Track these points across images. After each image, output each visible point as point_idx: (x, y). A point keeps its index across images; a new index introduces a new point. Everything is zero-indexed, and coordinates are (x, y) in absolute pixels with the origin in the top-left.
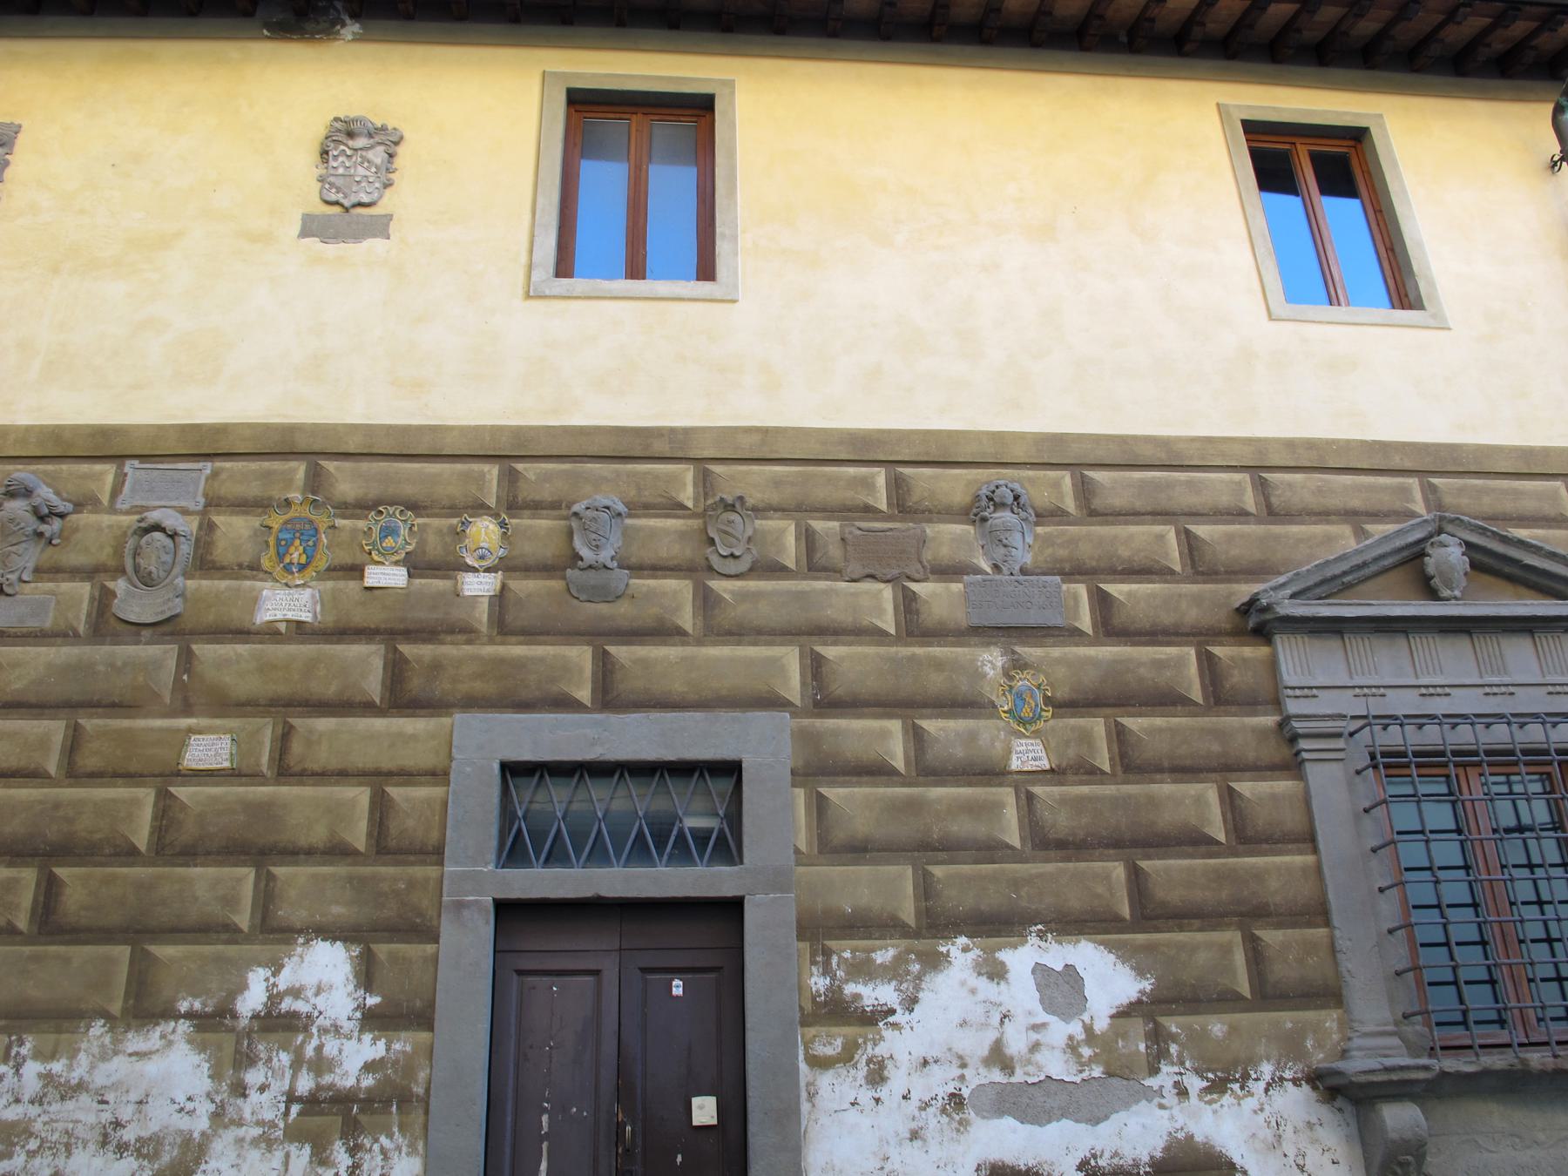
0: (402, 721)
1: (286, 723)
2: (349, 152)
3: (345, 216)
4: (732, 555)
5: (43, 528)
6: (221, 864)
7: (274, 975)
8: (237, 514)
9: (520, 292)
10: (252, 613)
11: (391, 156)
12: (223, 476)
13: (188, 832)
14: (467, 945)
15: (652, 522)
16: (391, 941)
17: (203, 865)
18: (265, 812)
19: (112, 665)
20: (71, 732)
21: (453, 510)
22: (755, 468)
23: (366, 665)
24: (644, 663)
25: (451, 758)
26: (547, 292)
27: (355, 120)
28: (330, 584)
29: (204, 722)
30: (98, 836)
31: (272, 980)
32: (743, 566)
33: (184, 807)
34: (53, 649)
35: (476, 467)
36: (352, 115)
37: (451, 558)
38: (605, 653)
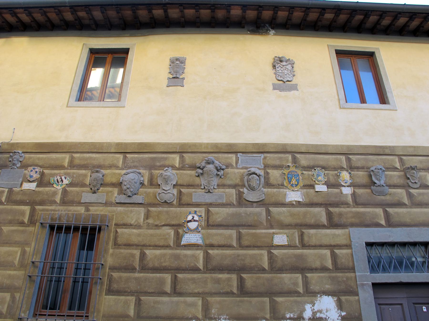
0: (334, 230)
1: (301, 231)
2: (282, 66)
3: (284, 84)
4: (415, 183)
5: (219, 173)
6: (291, 273)
7: (313, 306)
8: (274, 169)
9: (338, 107)
10: (285, 198)
11: (293, 67)
12: (268, 158)
13: (279, 264)
14: (366, 296)
15: (390, 173)
16: (345, 296)
17: (285, 274)
18: (300, 257)
19: (246, 214)
20: (238, 234)
21: (335, 169)
22: (414, 157)
23: (320, 214)
24: (397, 213)
25: (351, 241)
26: (346, 107)
27: (282, 57)
28: (305, 190)
29: (277, 231)
30: (253, 265)
31: (313, 308)
32: (418, 186)
33: (276, 256)
34: (228, 209)
35: (339, 157)
36: (280, 56)
37: (337, 183)
38: (386, 210)
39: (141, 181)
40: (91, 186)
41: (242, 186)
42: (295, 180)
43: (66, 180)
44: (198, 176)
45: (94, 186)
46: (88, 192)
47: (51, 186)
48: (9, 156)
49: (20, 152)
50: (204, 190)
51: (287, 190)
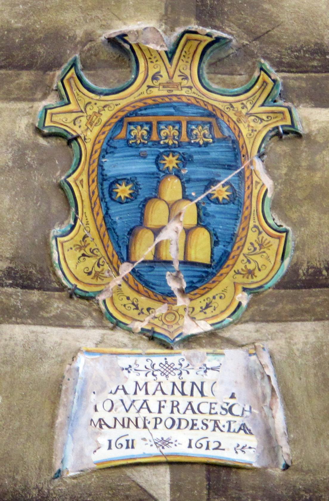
10: (48, 435)
28: (304, 334)
42: (189, 212)
51: (89, 336)
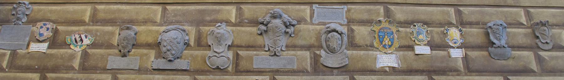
5: (288, 30)
28: (401, 53)
39: (186, 41)
40: (120, 47)
41: (318, 47)
42: (388, 39)
43: (87, 39)
44: (261, 34)
45: (124, 48)
46: (116, 55)
47: (67, 47)
48: (11, 7)
49: (27, 2)
50: (268, 53)
